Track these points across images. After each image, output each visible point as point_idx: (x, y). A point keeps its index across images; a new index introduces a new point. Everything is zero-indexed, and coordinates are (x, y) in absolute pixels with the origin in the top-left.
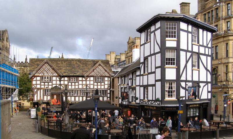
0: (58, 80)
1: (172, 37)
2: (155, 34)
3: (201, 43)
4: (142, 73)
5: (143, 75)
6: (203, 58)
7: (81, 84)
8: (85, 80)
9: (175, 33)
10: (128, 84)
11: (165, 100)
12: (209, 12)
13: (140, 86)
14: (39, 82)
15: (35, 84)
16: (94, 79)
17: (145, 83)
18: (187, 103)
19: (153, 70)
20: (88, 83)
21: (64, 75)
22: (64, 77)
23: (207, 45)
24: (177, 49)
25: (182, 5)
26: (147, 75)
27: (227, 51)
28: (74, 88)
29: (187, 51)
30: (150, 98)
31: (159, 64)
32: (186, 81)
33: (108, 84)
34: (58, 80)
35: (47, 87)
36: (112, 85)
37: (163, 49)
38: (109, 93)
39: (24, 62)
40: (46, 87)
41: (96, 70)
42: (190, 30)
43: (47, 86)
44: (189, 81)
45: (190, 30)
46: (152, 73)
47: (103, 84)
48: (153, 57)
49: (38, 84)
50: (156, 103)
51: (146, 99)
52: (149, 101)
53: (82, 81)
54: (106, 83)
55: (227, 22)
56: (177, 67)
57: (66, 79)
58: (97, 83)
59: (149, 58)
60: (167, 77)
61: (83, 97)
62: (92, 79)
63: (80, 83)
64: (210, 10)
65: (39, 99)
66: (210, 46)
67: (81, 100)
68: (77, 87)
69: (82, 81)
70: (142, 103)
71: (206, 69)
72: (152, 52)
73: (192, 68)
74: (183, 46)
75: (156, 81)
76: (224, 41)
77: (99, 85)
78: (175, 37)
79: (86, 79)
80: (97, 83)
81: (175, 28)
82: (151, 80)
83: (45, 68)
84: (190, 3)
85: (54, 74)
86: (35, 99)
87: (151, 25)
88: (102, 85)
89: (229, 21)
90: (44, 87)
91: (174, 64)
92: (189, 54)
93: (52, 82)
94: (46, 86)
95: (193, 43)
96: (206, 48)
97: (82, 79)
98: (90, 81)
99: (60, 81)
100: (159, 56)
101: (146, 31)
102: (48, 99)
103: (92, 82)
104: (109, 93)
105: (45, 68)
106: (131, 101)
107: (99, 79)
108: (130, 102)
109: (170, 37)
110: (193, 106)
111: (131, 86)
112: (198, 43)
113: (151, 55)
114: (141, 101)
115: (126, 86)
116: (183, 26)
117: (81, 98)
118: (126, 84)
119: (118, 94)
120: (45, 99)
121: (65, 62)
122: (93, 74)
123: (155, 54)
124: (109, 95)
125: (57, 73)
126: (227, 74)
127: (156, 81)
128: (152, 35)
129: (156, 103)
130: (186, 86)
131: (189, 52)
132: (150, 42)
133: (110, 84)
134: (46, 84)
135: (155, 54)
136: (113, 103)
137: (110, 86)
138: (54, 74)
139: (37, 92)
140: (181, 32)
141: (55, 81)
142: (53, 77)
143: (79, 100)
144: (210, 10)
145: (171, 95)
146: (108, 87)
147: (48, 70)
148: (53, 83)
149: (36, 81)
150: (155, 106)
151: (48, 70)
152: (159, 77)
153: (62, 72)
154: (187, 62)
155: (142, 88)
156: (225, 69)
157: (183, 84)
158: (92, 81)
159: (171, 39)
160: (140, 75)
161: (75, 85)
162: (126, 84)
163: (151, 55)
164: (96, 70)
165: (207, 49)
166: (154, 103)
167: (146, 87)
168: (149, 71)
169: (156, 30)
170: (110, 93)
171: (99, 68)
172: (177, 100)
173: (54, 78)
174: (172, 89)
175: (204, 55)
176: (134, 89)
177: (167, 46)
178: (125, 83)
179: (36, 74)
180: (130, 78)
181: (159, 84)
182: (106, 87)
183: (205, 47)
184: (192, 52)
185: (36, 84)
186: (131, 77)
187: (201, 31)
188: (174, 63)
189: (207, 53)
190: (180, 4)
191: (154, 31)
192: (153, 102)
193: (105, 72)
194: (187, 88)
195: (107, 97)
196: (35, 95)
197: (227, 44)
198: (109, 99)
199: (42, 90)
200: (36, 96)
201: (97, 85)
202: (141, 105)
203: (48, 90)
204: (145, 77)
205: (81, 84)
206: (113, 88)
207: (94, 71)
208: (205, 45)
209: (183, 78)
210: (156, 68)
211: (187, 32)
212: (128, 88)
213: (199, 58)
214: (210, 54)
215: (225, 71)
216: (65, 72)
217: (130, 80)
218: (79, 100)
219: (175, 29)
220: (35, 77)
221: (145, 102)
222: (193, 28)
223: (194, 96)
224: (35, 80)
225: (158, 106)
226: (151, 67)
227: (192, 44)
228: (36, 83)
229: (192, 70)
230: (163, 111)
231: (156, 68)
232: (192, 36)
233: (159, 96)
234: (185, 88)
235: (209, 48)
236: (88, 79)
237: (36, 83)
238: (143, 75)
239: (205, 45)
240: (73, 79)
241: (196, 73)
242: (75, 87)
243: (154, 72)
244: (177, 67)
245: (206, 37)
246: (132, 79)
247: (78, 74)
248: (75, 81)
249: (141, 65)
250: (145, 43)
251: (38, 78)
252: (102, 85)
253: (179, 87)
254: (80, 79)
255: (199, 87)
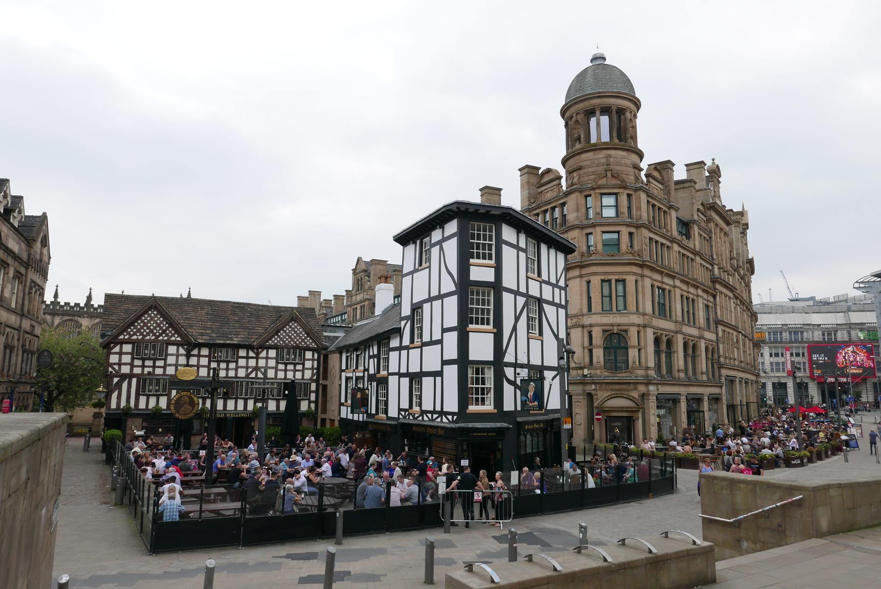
0: (182, 355)
1: (484, 258)
2: (441, 249)
3: (545, 276)
4: (406, 341)
5: (407, 348)
6: (549, 310)
7: (242, 367)
8: (254, 355)
9: (490, 249)
10: (366, 370)
11: (468, 411)
12: (545, 211)
13: (401, 375)
14: (126, 359)
15: (115, 364)
16: (277, 353)
17: (414, 368)
18: (519, 419)
19: (437, 336)
20: (262, 363)
21: (200, 341)
22: (200, 346)
23: (558, 281)
24: (497, 287)
25: (485, 191)
26: (421, 347)
27: (589, 298)
28: (224, 375)
29: (516, 293)
30: (427, 405)
31: (452, 320)
32: (515, 365)
33: (313, 369)
34: (182, 355)
35: (149, 373)
36: (323, 371)
37: (465, 287)
38: (313, 392)
39: (82, 305)
40: (146, 372)
41: (285, 332)
42: (522, 244)
43: (151, 370)
44: (522, 366)
45: (522, 244)
46: (432, 343)
47: (299, 367)
48: (437, 304)
49: (125, 364)
50: (445, 420)
51: (416, 409)
52: (423, 412)
53: (247, 358)
54: (308, 364)
55: (587, 234)
56: (495, 330)
57: (205, 351)
58: (295, 367)
59: (427, 306)
60: (474, 354)
61: (246, 401)
62: (272, 353)
63: (242, 362)
64: (549, 207)
65: (123, 404)
66: (562, 283)
67: (241, 407)
68: (232, 374)
69: (247, 358)
70: (404, 417)
71: (556, 337)
72: (435, 293)
73: (528, 333)
74: (509, 280)
75: (444, 363)
76: (581, 276)
77: (291, 370)
78: (490, 258)
79: (258, 354)
80: (295, 367)
81: (491, 237)
82: (431, 359)
83: (149, 322)
84: (500, 190)
85: (171, 337)
86: (113, 405)
87: (434, 228)
88: (298, 371)
89: (591, 233)
90: (143, 370)
91: (488, 324)
92: (521, 300)
93: (165, 360)
94: (146, 370)
95: (530, 274)
96: (525, 292)
97: (248, 353)
98: (267, 358)
99: (188, 356)
100: (452, 303)
101: (418, 242)
102: (150, 407)
103: (272, 363)
104: (313, 392)
105: (149, 322)
106: (374, 412)
107: (290, 354)
108: (370, 415)
109: (478, 258)
110: (531, 427)
111: (375, 374)
112: (539, 275)
113: (430, 299)
114: (403, 413)
115: (361, 374)
116: (508, 233)
117: (241, 403)
118: (361, 368)
119: (337, 393)
120: (142, 405)
121: (202, 309)
122: (275, 340)
123: (441, 297)
124: (313, 397)
125: (178, 332)
126: (591, 351)
127: (444, 363)
128: (435, 251)
129: (445, 420)
130: (515, 377)
131: (522, 295)
132: (429, 267)
133: (318, 368)
134: (149, 363)
135: (441, 297)
136: (324, 416)
137: (318, 374)
138: (173, 339)
139: (119, 386)
140: (505, 249)
141: (201, 364)
142: (170, 347)
143: (236, 407)
144: (549, 207)
145: (483, 400)
146: (313, 375)
147: (295, 337)
148: (168, 362)
149: (121, 353)
150: (442, 428)
151: (295, 337)
152: (451, 352)
153: (196, 334)
154: (517, 319)
155: (405, 381)
156: (586, 339)
157: (509, 372)
158: (271, 358)
159: (481, 261)
160: (400, 348)
161: (227, 369)
162: (361, 368)
163: (430, 299)
164: (285, 332)
165: (557, 290)
166: (439, 420)
167: (416, 378)
168: (426, 338)
169: (445, 239)
170: (317, 392)
171: (290, 327)
172: (496, 411)
173: (172, 349)
174: (483, 383)
175: (552, 303)
176: (383, 382)
177: (472, 278)
178: (357, 367)
179: (122, 337)
180: (371, 354)
181: (451, 372)
182: (308, 374)
183: (555, 286)
184: (527, 295)
185: (120, 364)
186: (376, 353)
187: (544, 248)
188: (488, 319)
189: (557, 301)
190: (481, 190)
191: (440, 243)
192: (435, 416)
193: (306, 338)
194: (518, 382)
195: (309, 399)
196: (112, 392)
197: (589, 282)
198: (313, 406)
199: (134, 380)
200: (115, 395)
201: (286, 370)
202: (401, 423)
203: (151, 380)
204: (415, 353)
205: (242, 367)
206: (325, 377)
207: (721, 366)
208: (553, 280)
209: (509, 358)
210: (444, 330)
211: (517, 247)
212: (366, 379)
213: (541, 310)
214: (563, 303)
215: (586, 344)
216: (202, 334)
217: (371, 360)
218: (236, 407)
219: (491, 240)
220: (116, 344)
221: (413, 417)
222: (529, 239)
223: (536, 403)
224: (116, 353)
225: (449, 426)
226: (431, 328)
227: (528, 278)
228: (120, 360)
229: (528, 339)
230: (464, 441)
231: (444, 330)
232: (527, 258)
233: (452, 405)
234: (512, 383)
235: (561, 288)
236: (263, 354)
237: (120, 360)
238: (407, 348)
239: (553, 280)
240: (222, 354)
241: (535, 344)
242: (227, 374)
243: (440, 342)
244: (495, 330)
245: (553, 263)
246: (378, 356)
247: (235, 341)
248: (227, 357)
249: (403, 323)
250: (416, 271)
251: (127, 348)
252: (298, 371)
253: (500, 377)
254: (243, 353)
255: (542, 379)
